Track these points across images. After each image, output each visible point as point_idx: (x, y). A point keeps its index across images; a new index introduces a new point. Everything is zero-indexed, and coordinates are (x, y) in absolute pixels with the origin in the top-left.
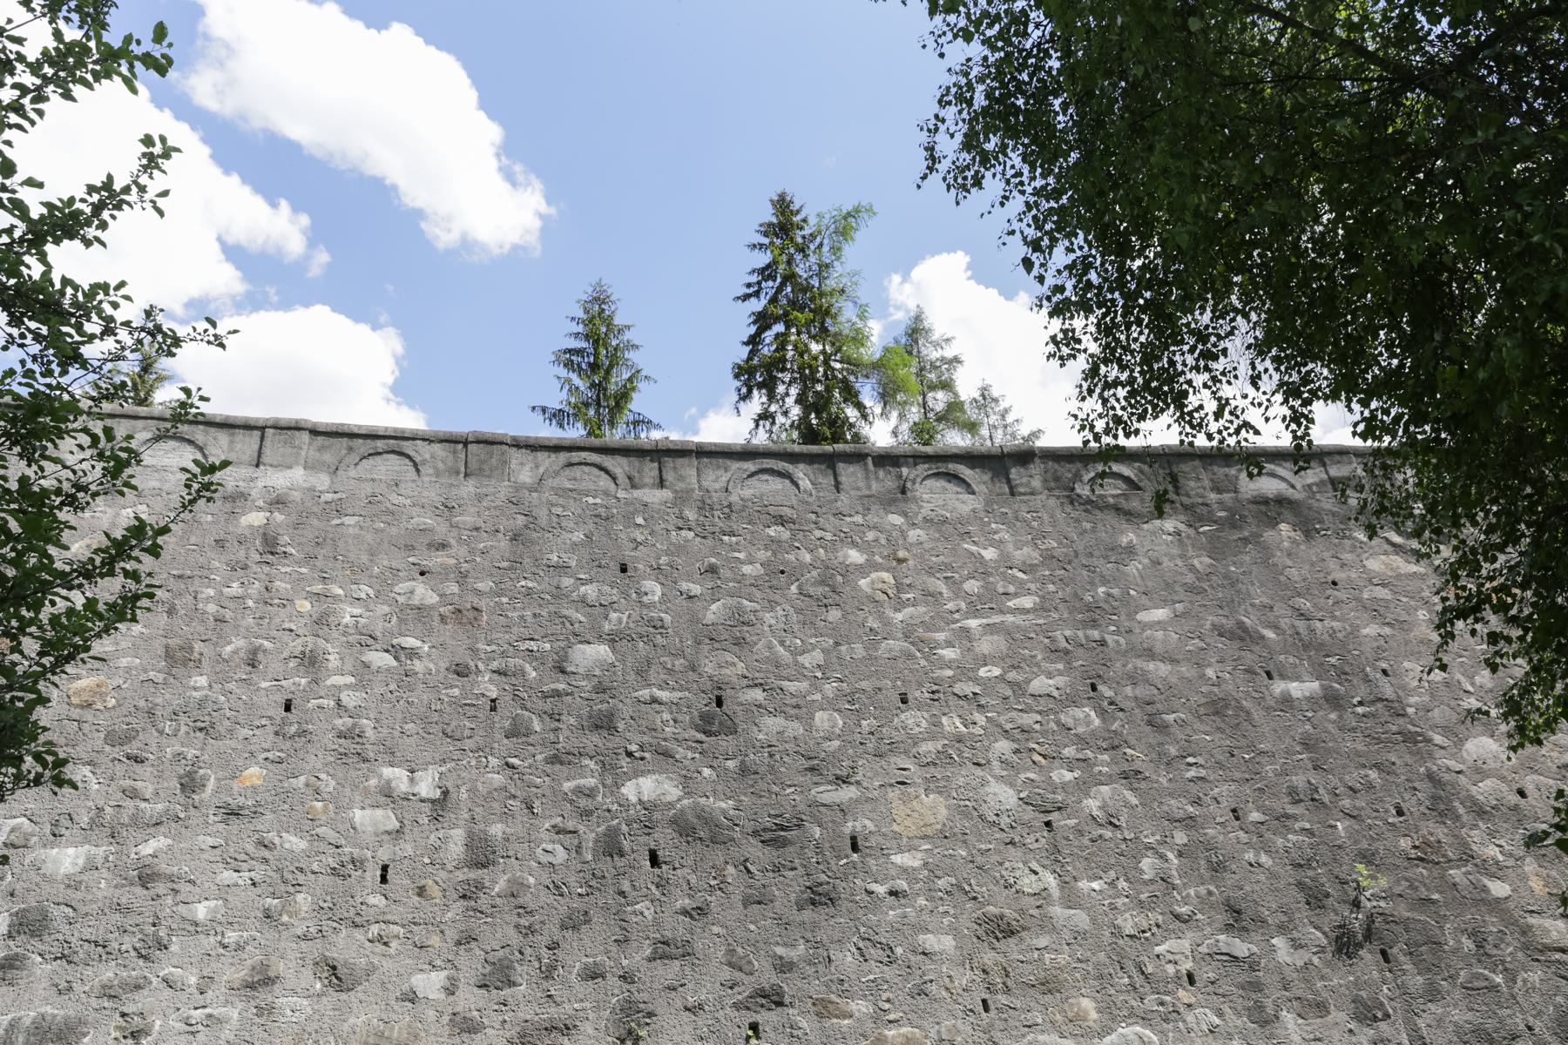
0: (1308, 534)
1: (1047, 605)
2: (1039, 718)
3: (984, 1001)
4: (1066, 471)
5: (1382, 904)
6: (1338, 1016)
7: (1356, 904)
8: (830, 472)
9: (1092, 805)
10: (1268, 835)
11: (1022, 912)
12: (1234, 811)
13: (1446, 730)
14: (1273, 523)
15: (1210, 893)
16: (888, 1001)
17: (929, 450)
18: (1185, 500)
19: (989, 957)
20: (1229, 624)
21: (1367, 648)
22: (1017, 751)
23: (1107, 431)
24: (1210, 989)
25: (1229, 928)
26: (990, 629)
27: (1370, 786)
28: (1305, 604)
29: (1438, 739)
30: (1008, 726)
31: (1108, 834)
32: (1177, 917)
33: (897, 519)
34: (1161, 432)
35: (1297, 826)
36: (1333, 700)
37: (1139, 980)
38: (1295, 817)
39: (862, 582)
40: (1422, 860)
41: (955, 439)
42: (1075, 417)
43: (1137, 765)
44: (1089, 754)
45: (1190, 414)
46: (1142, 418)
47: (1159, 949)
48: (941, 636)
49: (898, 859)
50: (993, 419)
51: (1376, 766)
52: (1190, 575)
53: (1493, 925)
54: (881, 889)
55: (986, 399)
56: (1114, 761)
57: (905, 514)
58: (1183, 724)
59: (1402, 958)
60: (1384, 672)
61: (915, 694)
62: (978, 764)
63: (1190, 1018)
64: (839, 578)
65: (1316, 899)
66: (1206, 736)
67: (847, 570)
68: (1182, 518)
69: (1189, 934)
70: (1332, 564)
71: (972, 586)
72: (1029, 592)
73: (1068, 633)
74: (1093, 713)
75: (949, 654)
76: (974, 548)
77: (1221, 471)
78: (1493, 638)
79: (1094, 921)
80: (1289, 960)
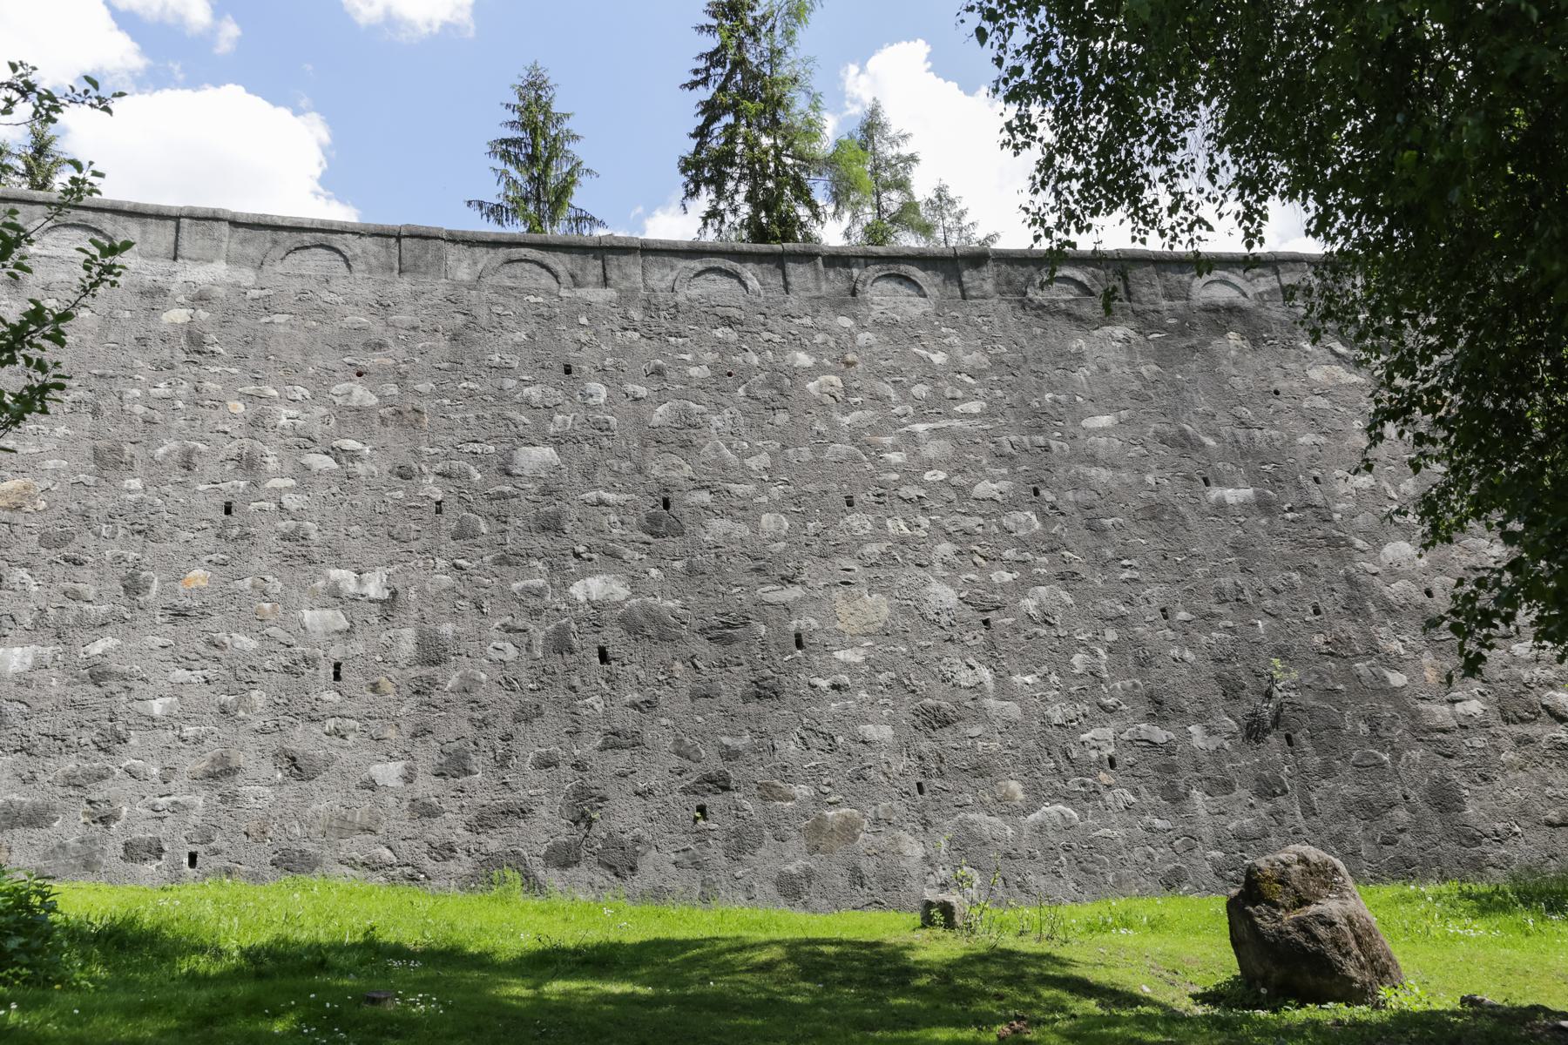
0: (1255, 343)
1: (994, 410)
2: (981, 521)
3: (919, 785)
4: (1019, 275)
5: (1292, 694)
6: (1241, 793)
7: (1268, 695)
8: (779, 272)
9: (1029, 604)
10: (1194, 633)
11: (958, 704)
12: (1163, 610)
13: (1368, 535)
14: (1222, 331)
15: (1135, 686)
16: (829, 785)
17: (880, 250)
18: (1137, 306)
19: (925, 746)
20: (1171, 431)
21: (1302, 457)
22: (959, 553)
23: (1059, 226)
24: (1129, 771)
25: (1150, 717)
26: (937, 433)
27: (1292, 587)
28: (1246, 413)
29: (1359, 543)
30: (951, 529)
31: (1043, 631)
32: (1103, 707)
33: (846, 322)
34: (1112, 232)
35: (1221, 624)
36: (1264, 506)
37: (1064, 764)
38: (1220, 616)
39: (810, 385)
41: (908, 241)
42: (1027, 210)
43: (1075, 567)
44: (1029, 556)
45: (1144, 209)
46: (1095, 212)
47: (1084, 737)
48: (888, 440)
49: (840, 655)
50: (949, 221)
51: (1299, 568)
52: (1137, 382)
53: (1388, 711)
54: (823, 683)
55: (942, 200)
56: (1052, 564)
57: (855, 317)
58: (1120, 528)
59: (1304, 742)
60: (1316, 480)
61: (860, 497)
62: (920, 565)
63: (1109, 797)
64: (787, 381)
65: (1232, 691)
66: (1141, 539)
67: (795, 374)
68: (1133, 324)
69: (1113, 723)
70: (1276, 374)
71: (921, 390)
72: (977, 397)
73: (1013, 438)
74: (1034, 517)
75: (895, 457)
76: (923, 352)
77: (1173, 277)
78: (1420, 439)
79: (1025, 712)
80: (1202, 745)
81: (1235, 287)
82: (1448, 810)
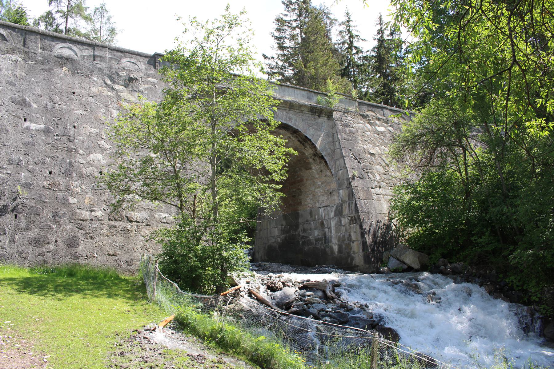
0: (73, 73)
7: (15, 200)
14: (61, 66)
18: (26, 50)
21: (72, 118)
29: (81, 152)
36: (47, 131)
38: (6, 169)
40: (49, 189)
51: (51, 157)
55: (102, 10)
68: (22, 56)
77: (47, 42)
81: (74, 51)
82: (71, 247)
